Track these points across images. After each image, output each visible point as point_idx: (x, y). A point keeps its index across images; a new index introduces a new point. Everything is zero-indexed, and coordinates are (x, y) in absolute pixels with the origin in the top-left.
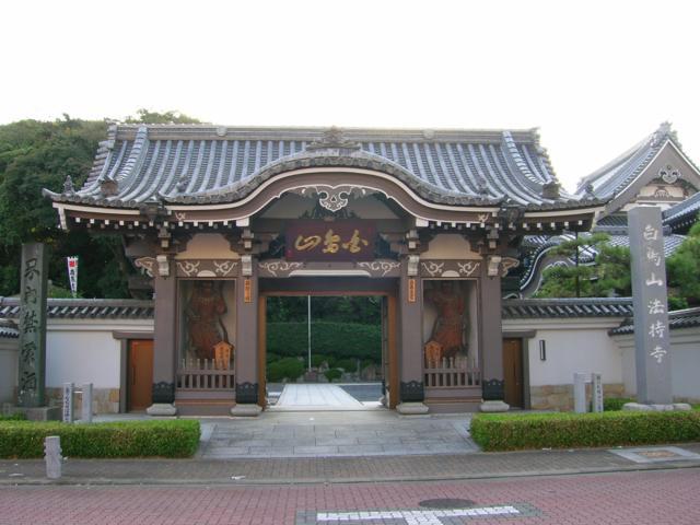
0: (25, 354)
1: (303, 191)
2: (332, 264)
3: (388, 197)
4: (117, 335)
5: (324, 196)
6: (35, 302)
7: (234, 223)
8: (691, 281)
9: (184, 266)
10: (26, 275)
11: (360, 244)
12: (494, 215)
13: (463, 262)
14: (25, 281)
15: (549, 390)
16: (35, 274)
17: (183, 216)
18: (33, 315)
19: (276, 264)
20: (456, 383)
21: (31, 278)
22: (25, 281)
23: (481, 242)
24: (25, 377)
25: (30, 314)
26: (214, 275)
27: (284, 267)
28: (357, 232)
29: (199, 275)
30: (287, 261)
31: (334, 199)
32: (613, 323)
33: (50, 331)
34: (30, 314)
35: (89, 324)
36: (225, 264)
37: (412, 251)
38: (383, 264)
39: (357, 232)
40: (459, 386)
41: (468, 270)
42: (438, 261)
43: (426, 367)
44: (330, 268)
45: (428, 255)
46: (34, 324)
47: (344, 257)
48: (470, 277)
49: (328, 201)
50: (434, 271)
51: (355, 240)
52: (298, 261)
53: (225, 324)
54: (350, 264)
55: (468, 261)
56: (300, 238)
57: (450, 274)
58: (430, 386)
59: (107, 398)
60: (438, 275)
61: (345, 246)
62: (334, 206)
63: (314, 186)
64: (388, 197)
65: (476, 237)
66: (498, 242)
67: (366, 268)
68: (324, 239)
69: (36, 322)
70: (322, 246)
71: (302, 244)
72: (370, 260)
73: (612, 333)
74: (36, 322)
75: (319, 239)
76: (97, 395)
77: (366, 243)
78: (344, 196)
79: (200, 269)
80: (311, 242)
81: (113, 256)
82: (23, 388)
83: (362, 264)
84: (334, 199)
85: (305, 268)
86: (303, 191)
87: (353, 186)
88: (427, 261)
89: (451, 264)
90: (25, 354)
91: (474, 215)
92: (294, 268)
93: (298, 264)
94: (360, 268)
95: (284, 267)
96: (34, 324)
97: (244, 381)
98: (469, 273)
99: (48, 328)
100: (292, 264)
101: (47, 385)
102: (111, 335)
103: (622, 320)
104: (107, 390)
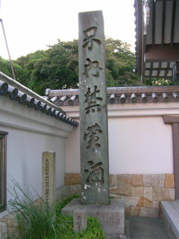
0: (88, 139)
4: (168, 120)
6: (97, 76)
8: (95, 133)
10: (84, 46)
14: (84, 53)
21: (90, 49)
22: (84, 53)
24: (89, 167)
25: (92, 90)
34: (92, 90)
35: (140, 108)
46: (98, 102)
53: (44, 137)
59: (162, 185)
69: (101, 99)
74: (101, 99)
76: (154, 180)
81: (38, 73)
82: (88, 181)
90: (88, 139)
96: (98, 102)
99: (109, 114)
102: (160, 120)
104: (162, 175)
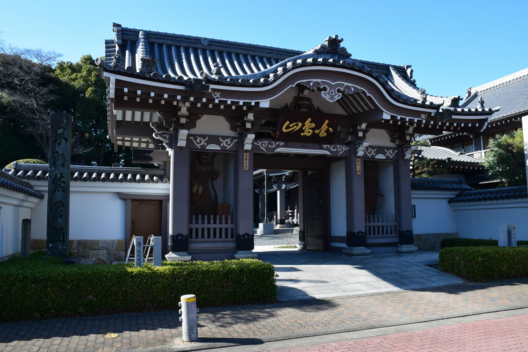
1: (311, 84)
2: (306, 144)
3: (368, 95)
5: (325, 89)
7: (257, 104)
9: (196, 140)
11: (327, 131)
12: (433, 115)
13: (388, 148)
15: (418, 236)
16: (63, 140)
17: (218, 95)
18: (62, 177)
19: (266, 142)
20: (221, 237)
21: (59, 144)
23: (238, 124)
25: (59, 175)
26: (220, 149)
27: (272, 145)
28: (327, 121)
29: (208, 148)
30: (274, 140)
31: (332, 93)
32: (452, 195)
33: (72, 186)
34: (59, 175)
36: (228, 140)
37: (183, 126)
38: (339, 146)
39: (327, 121)
40: (376, 235)
41: (228, 145)
42: (203, 136)
43: (191, 222)
44: (304, 147)
45: (193, 131)
47: (315, 140)
48: (228, 151)
49: (328, 93)
50: (199, 143)
51: (325, 127)
52: (282, 141)
54: (317, 145)
55: (227, 137)
56: (288, 123)
57: (380, 156)
58: (194, 239)
60: (203, 147)
61: (316, 131)
62: (332, 98)
63: (319, 80)
64: (368, 95)
65: (236, 117)
66: (252, 123)
67: (328, 149)
68: (304, 125)
70: (301, 130)
71: (288, 127)
72: (331, 144)
73: (451, 201)
75: (300, 124)
77: (331, 130)
78: (339, 91)
79: (208, 143)
80: (295, 127)
83: (325, 146)
84: (332, 93)
85: (286, 146)
86: (311, 84)
87: (315, 80)
88: (195, 136)
89: (214, 139)
91: (418, 114)
92: (278, 146)
93: (282, 144)
94: (324, 149)
95: (272, 145)
97: (407, 229)
98: (229, 147)
100: (277, 143)
101: (332, 235)
103: (457, 193)
